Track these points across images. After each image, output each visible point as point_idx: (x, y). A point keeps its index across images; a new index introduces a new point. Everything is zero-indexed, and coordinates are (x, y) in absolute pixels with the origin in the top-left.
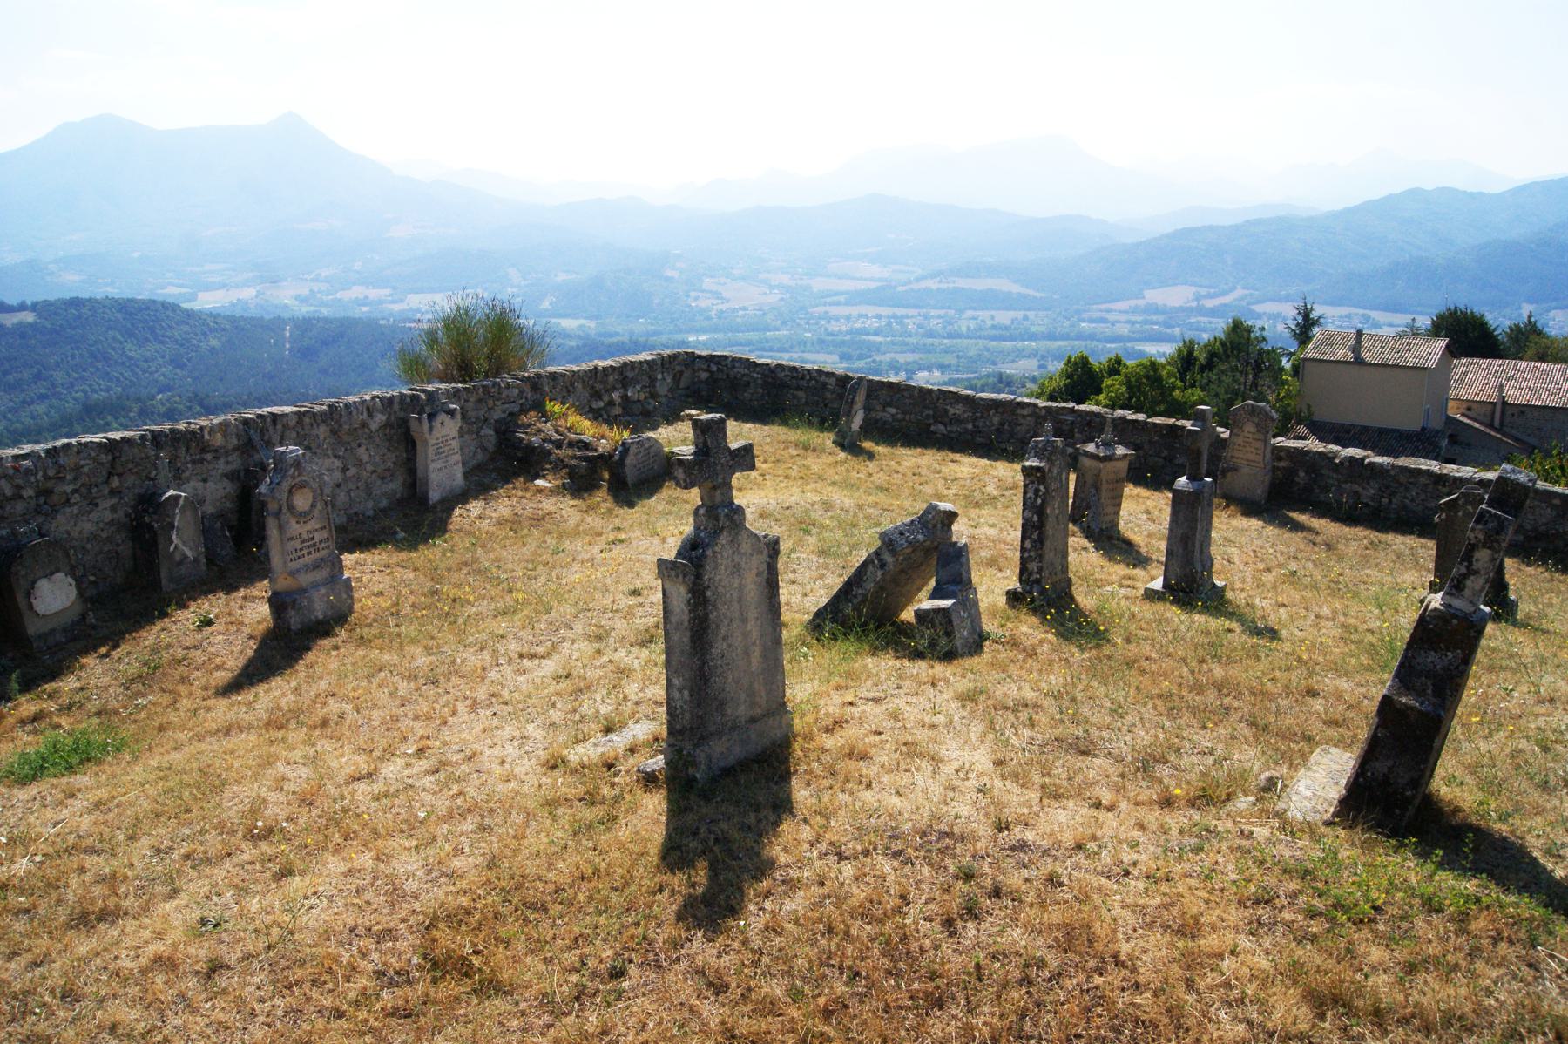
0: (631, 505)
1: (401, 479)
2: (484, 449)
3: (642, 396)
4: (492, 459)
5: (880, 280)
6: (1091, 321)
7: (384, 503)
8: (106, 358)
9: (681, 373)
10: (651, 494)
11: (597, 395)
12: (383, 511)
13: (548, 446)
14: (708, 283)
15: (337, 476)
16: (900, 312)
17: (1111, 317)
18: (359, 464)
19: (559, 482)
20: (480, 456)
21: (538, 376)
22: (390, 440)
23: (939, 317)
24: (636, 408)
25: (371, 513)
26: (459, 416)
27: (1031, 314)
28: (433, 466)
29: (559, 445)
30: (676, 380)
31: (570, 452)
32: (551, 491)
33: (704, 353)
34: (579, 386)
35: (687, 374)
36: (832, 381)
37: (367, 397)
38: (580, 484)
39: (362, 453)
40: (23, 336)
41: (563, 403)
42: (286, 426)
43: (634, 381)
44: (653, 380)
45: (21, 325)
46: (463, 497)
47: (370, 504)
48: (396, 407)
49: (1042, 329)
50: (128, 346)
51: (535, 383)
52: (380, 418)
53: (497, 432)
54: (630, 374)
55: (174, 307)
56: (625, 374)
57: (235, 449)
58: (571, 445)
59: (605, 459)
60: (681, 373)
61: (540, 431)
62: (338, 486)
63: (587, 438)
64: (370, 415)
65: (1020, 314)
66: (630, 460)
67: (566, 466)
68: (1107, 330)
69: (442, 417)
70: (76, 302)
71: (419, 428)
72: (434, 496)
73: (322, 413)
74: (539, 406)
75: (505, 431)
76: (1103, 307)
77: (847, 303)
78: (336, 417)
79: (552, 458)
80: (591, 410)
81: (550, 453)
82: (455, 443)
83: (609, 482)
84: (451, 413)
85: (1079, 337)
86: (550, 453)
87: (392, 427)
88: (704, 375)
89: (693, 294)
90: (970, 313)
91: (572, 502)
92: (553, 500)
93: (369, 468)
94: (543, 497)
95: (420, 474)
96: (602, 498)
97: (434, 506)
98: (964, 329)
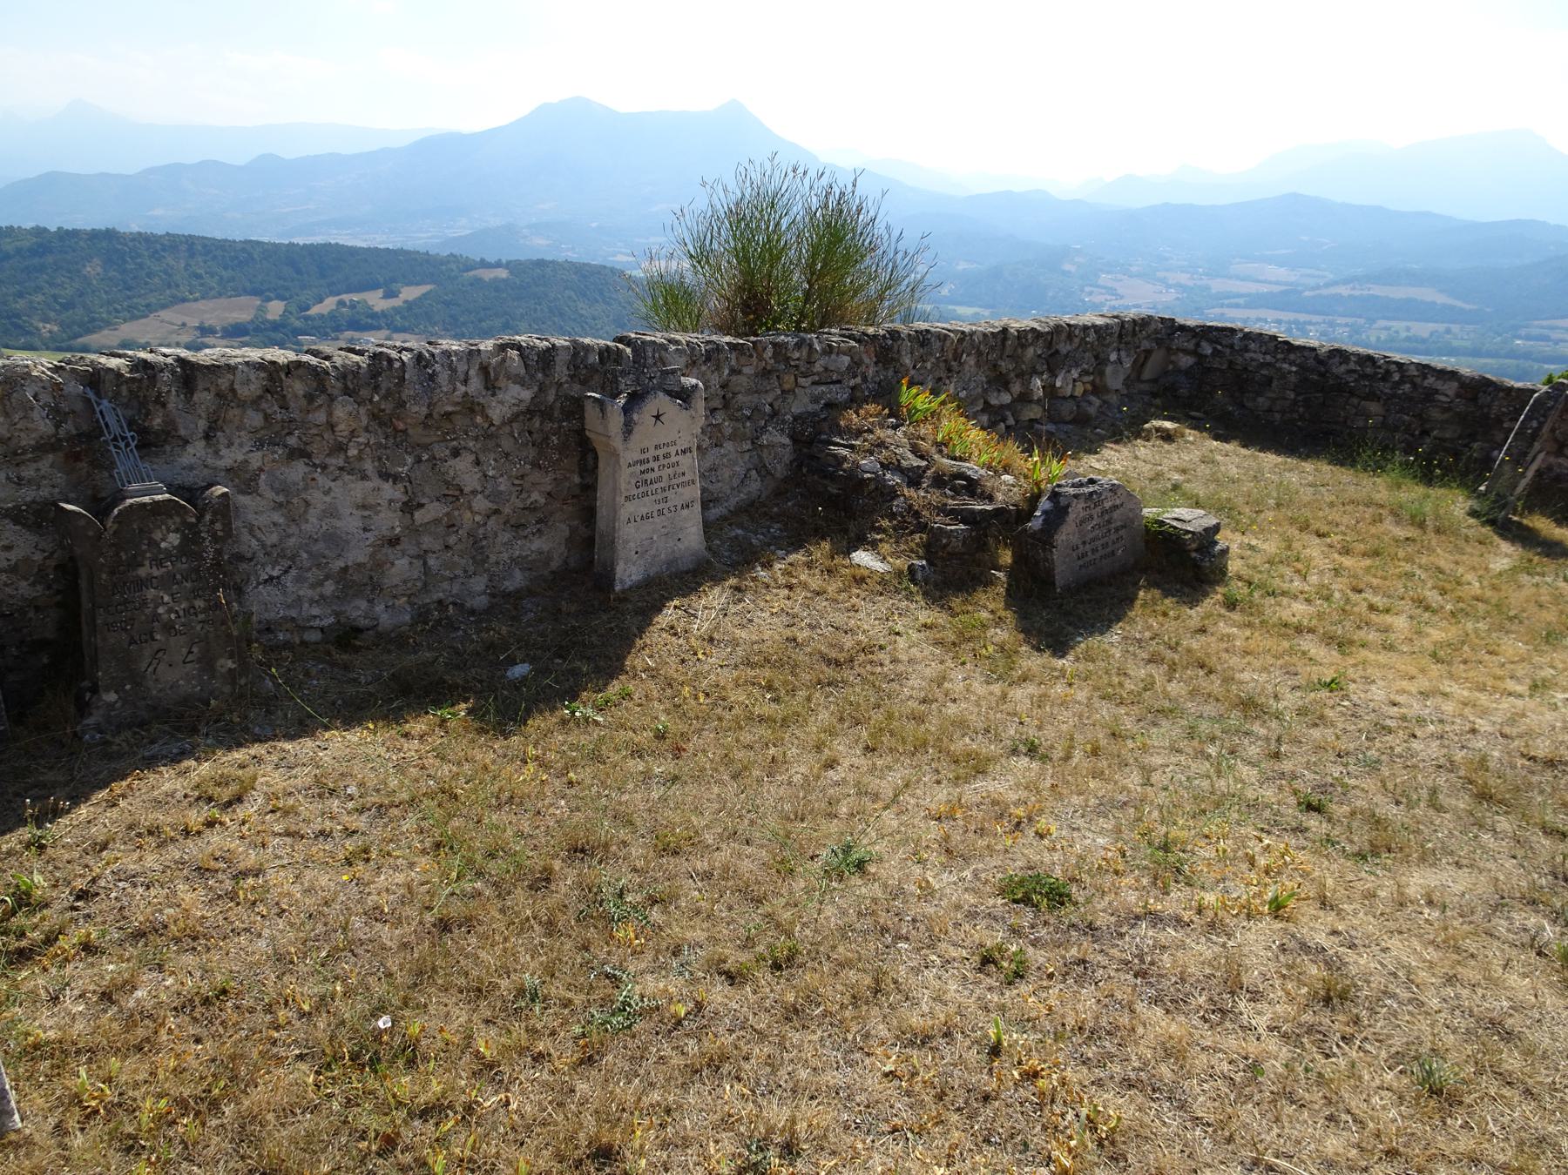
0: (1059, 647)
1: (563, 530)
2: (763, 470)
3: (1079, 391)
4: (779, 493)
5: (1286, 284)
6: (1528, 338)
7: (517, 580)
8: (561, 315)
9: (1148, 352)
10: (1103, 624)
11: (1001, 382)
12: (516, 596)
13: (893, 479)
14: (1104, 278)
15: (388, 521)
16: (1302, 317)
17: (1556, 335)
18: (454, 494)
19: (901, 563)
20: (755, 486)
21: (894, 335)
22: (541, 445)
23: (1347, 325)
24: (1067, 409)
25: (481, 602)
26: (700, 405)
27: (1455, 328)
28: (627, 510)
29: (914, 478)
30: (1139, 366)
31: (935, 497)
32: (883, 582)
33: (1191, 323)
34: (970, 361)
35: (1157, 357)
36: (1451, 388)
37: (487, 345)
38: (947, 573)
39: (463, 470)
40: (497, 290)
41: (935, 392)
42: (227, 397)
43: (1069, 361)
44: (1101, 361)
45: (496, 279)
46: (686, 579)
47: (479, 583)
48: (561, 372)
49: (1468, 344)
50: (580, 305)
51: (886, 349)
52: (516, 395)
53: (795, 439)
54: (1064, 348)
55: (621, 273)
56: (1057, 345)
57: (43, 447)
58: (939, 481)
59: (1011, 520)
60: (1148, 352)
61: (881, 444)
62: (394, 542)
63: (973, 469)
64: (491, 386)
65: (1441, 327)
66: (1066, 535)
67: (922, 528)
68: (1546, 348)
69: (660, 402)
70: (541, 263)
71: (606, 424)
72: (628, 572)
73: (345, 374)
74: (886, 395)
75: (811, 438)
76: (1545, 323)
77: (1247, 306)
78: (385, 383)
79: (898, 505)
80: (988, 407)
81: (893, 494)
82: (690, 464)
83: (1012, 572)
84: (684, 396)
85: (1512, 354)
86: (893, 494)
87: (547, 414)
88: (1186, 361)
89: (1087, 289)
90: (1383, 323)
91: (925, 616)
92: (884, 604)
93: (481, 503)
94: (859, 602)
95: (601, 524)
96: (989, 608)
97: (623, 598)
98: (1373, 339)
